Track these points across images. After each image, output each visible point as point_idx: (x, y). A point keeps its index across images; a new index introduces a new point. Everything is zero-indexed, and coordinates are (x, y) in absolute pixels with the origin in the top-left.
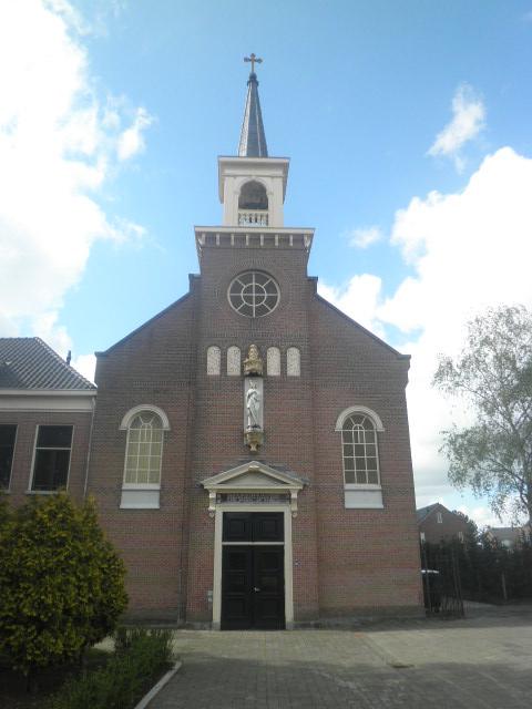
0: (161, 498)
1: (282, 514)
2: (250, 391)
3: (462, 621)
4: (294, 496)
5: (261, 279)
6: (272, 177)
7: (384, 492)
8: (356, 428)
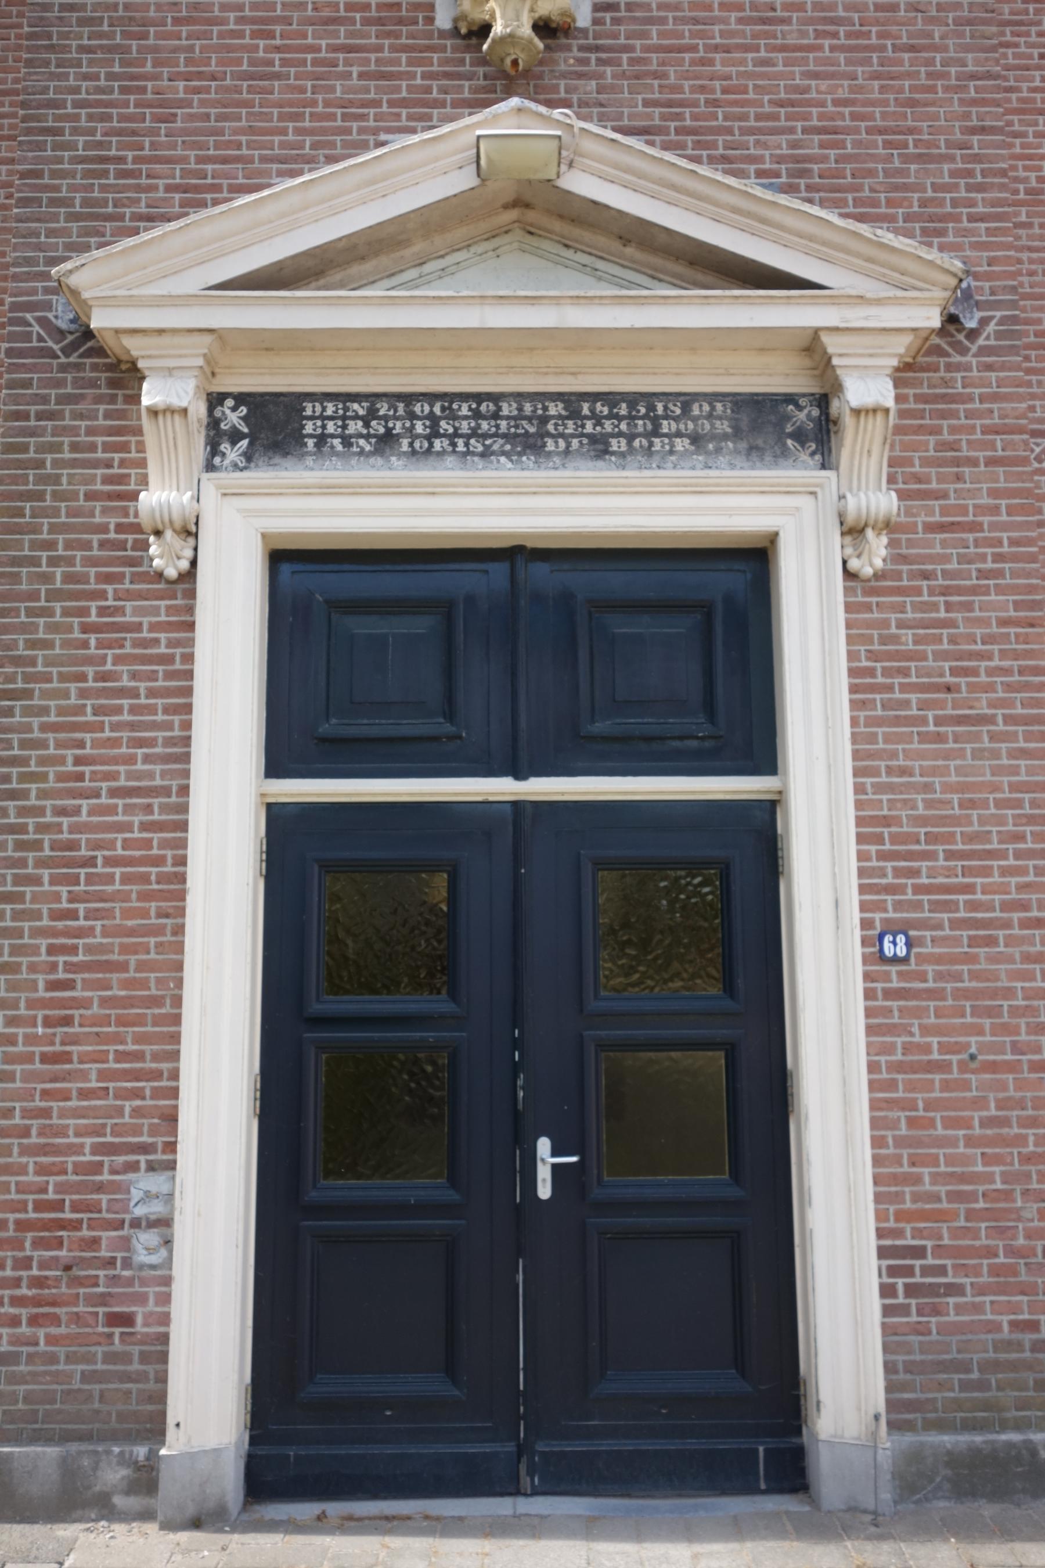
4: (867, 388)
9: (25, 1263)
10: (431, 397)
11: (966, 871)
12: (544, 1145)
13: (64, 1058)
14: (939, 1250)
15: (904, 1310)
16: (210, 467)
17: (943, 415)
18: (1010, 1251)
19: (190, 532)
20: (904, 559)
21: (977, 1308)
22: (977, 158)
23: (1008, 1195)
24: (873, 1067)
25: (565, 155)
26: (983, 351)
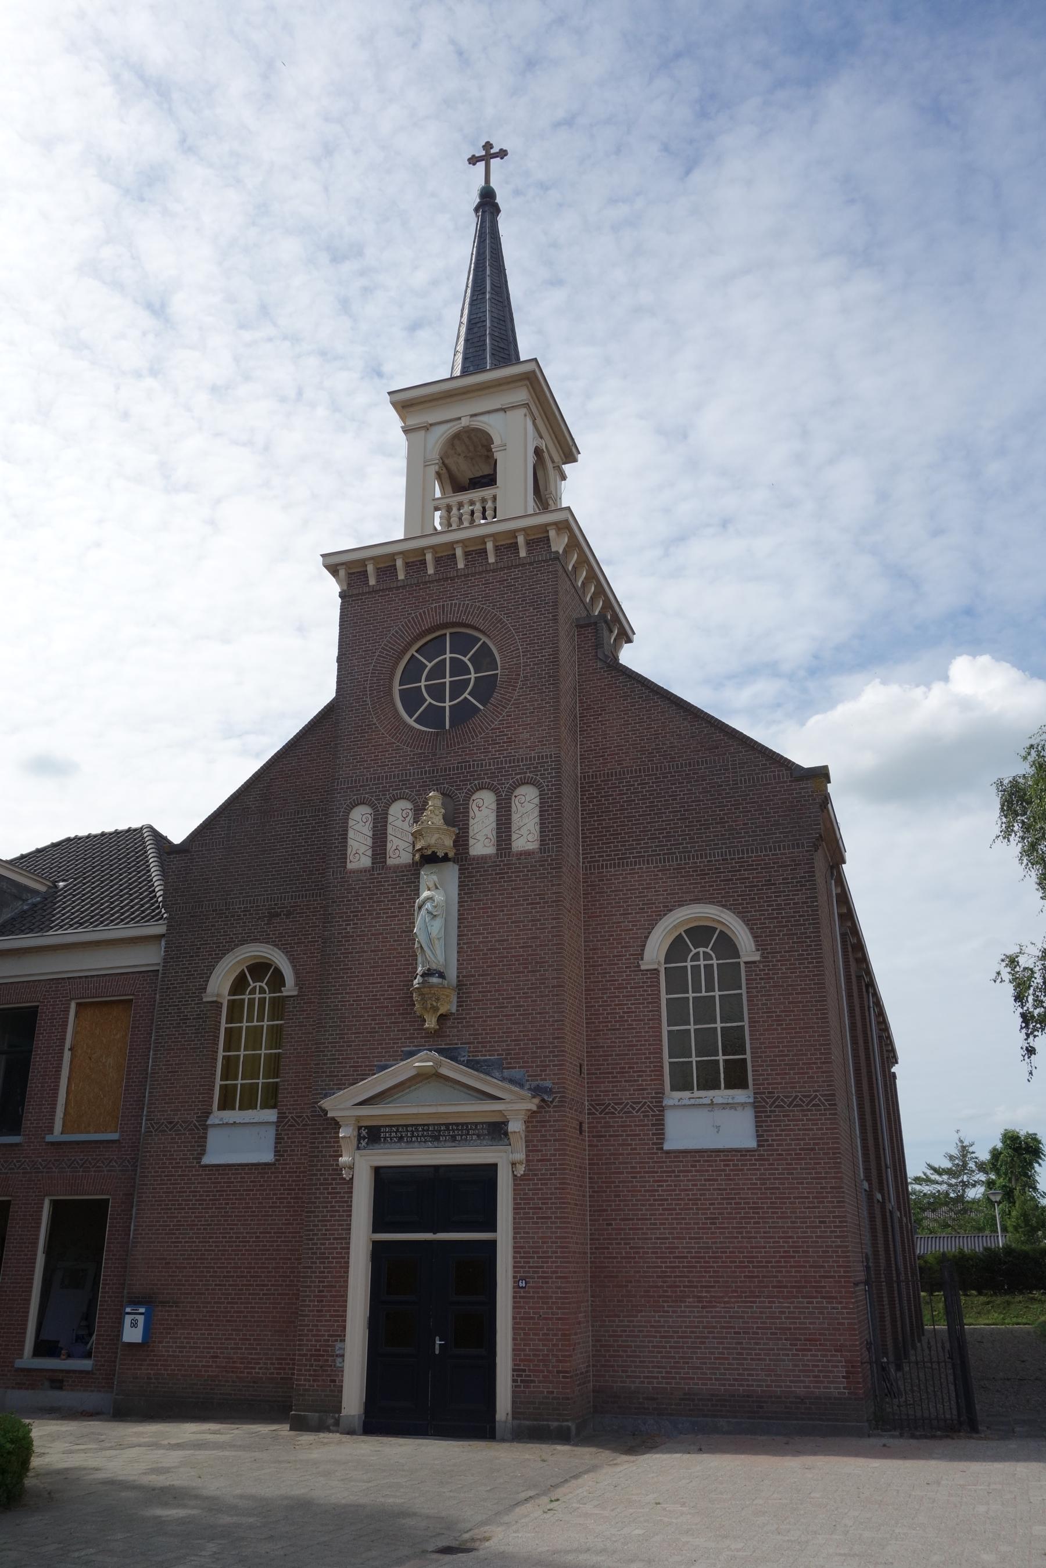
0: (278, 1139)
1: (494, 1167)
2: (425, 894)
3: (975, 1435)
4: (515, 1126)
5: (462, 643)
6: (504, 410)
7: (759, 1109)
8: (253, 992)
9: (312, 1365)
10: (412, 1125)
11: (542, 1262)
12: (437, 1338)
13: (321, 1311)
14: (530, 1370)
15: (520, 1386)
16: (358, 1148)
17: (543, 1126)
18: (549, 1371)
19: (351, 1168)
20: (530, 1170)
21: (539, 1387)
22: (556, 1047)
23: (547, 1355)
24: (514, 1318)
25: (439, 1064)
26: (555, 1107)
